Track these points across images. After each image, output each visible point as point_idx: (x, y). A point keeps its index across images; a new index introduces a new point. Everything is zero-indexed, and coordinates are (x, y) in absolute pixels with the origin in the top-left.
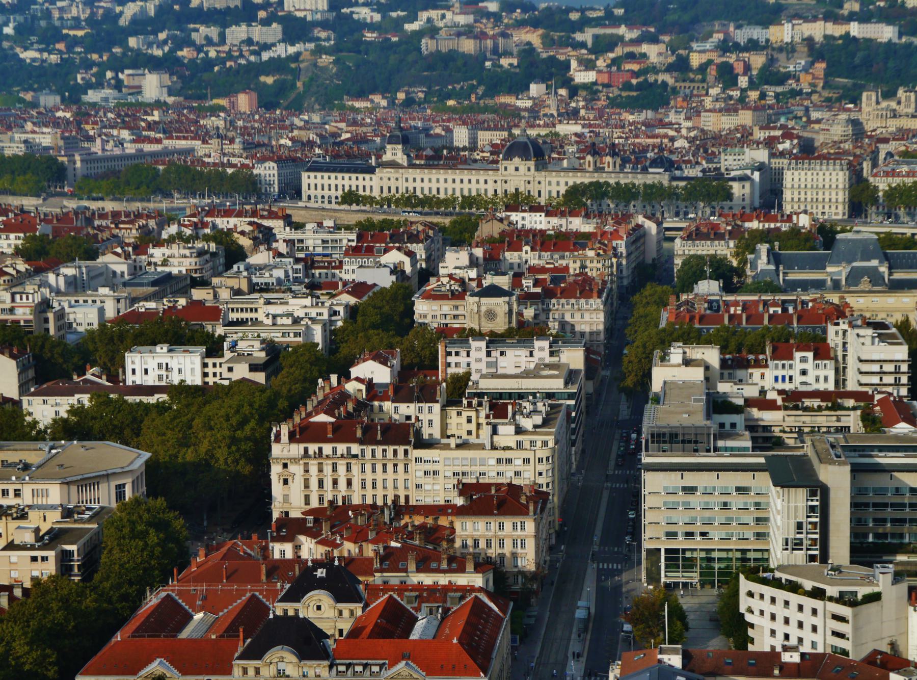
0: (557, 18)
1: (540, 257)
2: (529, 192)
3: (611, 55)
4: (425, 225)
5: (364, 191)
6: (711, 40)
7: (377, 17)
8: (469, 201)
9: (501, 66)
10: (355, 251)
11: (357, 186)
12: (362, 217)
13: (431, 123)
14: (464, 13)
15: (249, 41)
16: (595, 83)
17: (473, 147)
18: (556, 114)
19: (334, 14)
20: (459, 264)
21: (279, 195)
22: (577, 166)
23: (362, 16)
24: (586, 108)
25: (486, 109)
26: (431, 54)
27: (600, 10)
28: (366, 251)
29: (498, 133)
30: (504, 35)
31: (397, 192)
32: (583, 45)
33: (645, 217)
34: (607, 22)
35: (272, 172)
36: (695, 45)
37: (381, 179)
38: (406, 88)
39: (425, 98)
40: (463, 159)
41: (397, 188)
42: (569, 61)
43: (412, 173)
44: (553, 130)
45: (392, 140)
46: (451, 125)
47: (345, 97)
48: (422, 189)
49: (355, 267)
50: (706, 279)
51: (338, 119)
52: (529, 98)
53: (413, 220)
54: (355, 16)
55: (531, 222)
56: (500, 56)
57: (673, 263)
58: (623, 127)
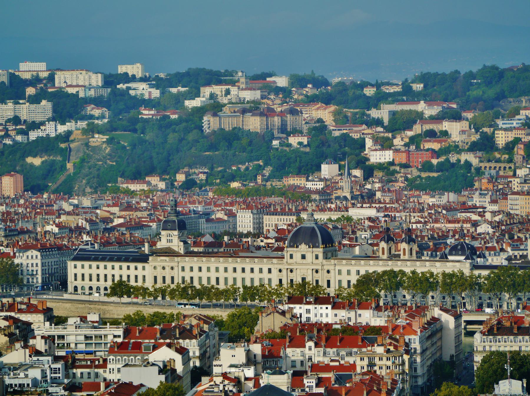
0: (351, 93)
1: (325, 354)
2: (317, 281)
3: (410, 133)
4: (200, 319)
5: (136, 281)
6: (517, 117)
7: (156, 93)
8: (251, 292)
9: (290, 145)
10: (121, 348)
11: (129, 276)
12: (131, 311)
13: (212, 206)
14: (250, 89)
15: (16, 120)
16: (392, 163)
17: (258, 233)
18: (349, 197)
19: (109, 90)
20: (235, 362)
21: (43, 287)
22: (370, 254)
23: (139, 92)
24: (382, 190)
25: (273, 192)
26: (214, 132)
27: (397, 85)
28: (133, 348)
29: (285, 217)
30: (293, 112)
31: (173, 282)
32: (379, 122)
33: (441, 309)
34: (405, 98)
35: (34, 262)
36: (500, 123)
37: (155, 268)
38: (186, 169)
39: (206, 180)
40: (246, 246)
41: (173, 278)
42: (364, 139)
43: (188, 262)
44: (345, 214)
45: (167, 225)
46: (234, 209)
47: (119, 179)
48: (200, 278)
49: (120, 366)
50: (507, 379)
51: (111, 203)
52: (321, 180)
53: (185, 313)
54: (132, 92)
55: (316, 315)
56: (288, 134)
57: (473, 361)
58: (422, 211)
